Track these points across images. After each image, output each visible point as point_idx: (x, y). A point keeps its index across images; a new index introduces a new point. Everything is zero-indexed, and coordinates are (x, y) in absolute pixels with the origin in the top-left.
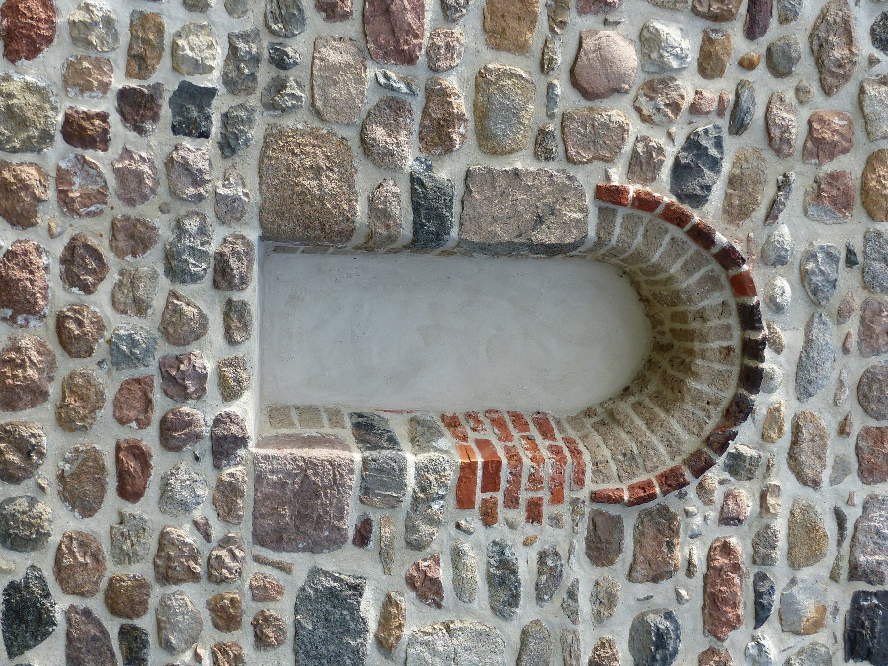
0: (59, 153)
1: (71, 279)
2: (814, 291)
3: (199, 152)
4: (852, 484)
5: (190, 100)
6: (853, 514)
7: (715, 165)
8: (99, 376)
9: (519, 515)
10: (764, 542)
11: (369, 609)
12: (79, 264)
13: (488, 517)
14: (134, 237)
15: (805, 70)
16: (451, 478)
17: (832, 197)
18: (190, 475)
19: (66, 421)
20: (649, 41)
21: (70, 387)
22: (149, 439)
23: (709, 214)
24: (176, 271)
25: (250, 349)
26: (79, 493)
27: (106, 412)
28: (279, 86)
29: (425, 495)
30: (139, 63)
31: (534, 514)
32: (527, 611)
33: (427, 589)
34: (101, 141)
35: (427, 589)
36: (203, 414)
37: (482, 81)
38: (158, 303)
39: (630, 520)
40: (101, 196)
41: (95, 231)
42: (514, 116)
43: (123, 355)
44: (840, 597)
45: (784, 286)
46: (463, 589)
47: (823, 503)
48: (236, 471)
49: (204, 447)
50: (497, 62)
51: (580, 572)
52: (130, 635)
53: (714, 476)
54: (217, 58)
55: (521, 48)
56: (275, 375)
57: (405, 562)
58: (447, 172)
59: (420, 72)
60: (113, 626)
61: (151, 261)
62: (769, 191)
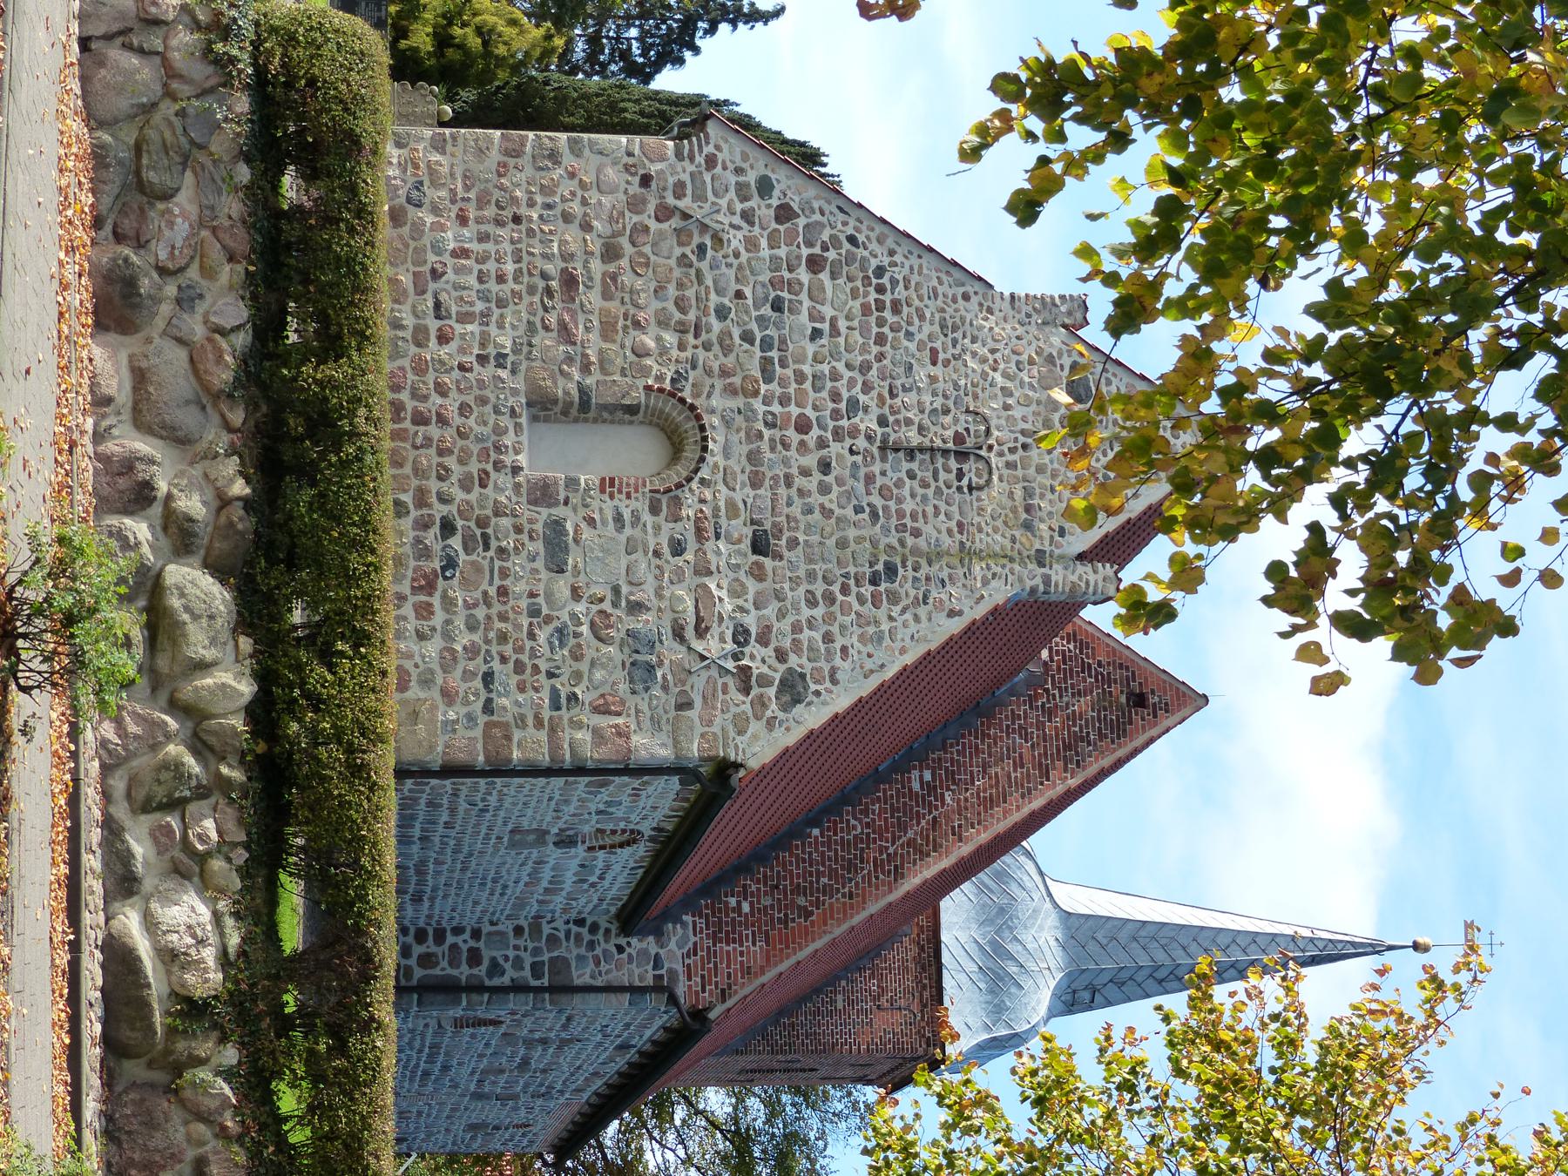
0: (456, 374)
1: (461, 414)
2: (727, 423)
3: (504, 374)
4: (748, 490)
5: (501, 360)
6: (750, 501)
7: (686, 379)
8: (472, 446)
9: (623, 496)
10: (716, 509)
11: (569, 527)
12: (464, 409)
13: (612, 497)
14: (483, 401)
15: (716, 348)
16: (597, 482)
17: (731, 391)
18: (504, 479)
19: (461, 462)
20: (659, 339)
21: (462, 450)
22: (489, 467)
23: (687, 394)
24: (497, 411)
25: (524, 438)
26: (466, 485)
27: (475, 458)
28: (530, 352)
29: (588, 489)
30: (483, 345)
31: (628, 496)
32: (628, 531)
33: (591, 522)
34: (470, 370)
35: (591, 522)
36: (508, 459)
37: (601, 352)
38: (491, 422)
39: (664, 500)
40: (471, 388)
41: (470, 399)
42: (612, 362)
43: (479, 440)
44: (748, 531)
45: (716, 421)
46: (604, 523)
47: (738, 497)
48: (520, 479)
49: (509, 470)
50: (605, 346)
51: (647, 517)
52: (483, 535)
53: (694, 485)
54: (509, 344)
55: (614, 341)
56: (536, 454)
57: (582, 512)
58: (588, 381)
59: (579, 349)
60: (478, 532)
61: (488, 409)
62: (707, 389)
